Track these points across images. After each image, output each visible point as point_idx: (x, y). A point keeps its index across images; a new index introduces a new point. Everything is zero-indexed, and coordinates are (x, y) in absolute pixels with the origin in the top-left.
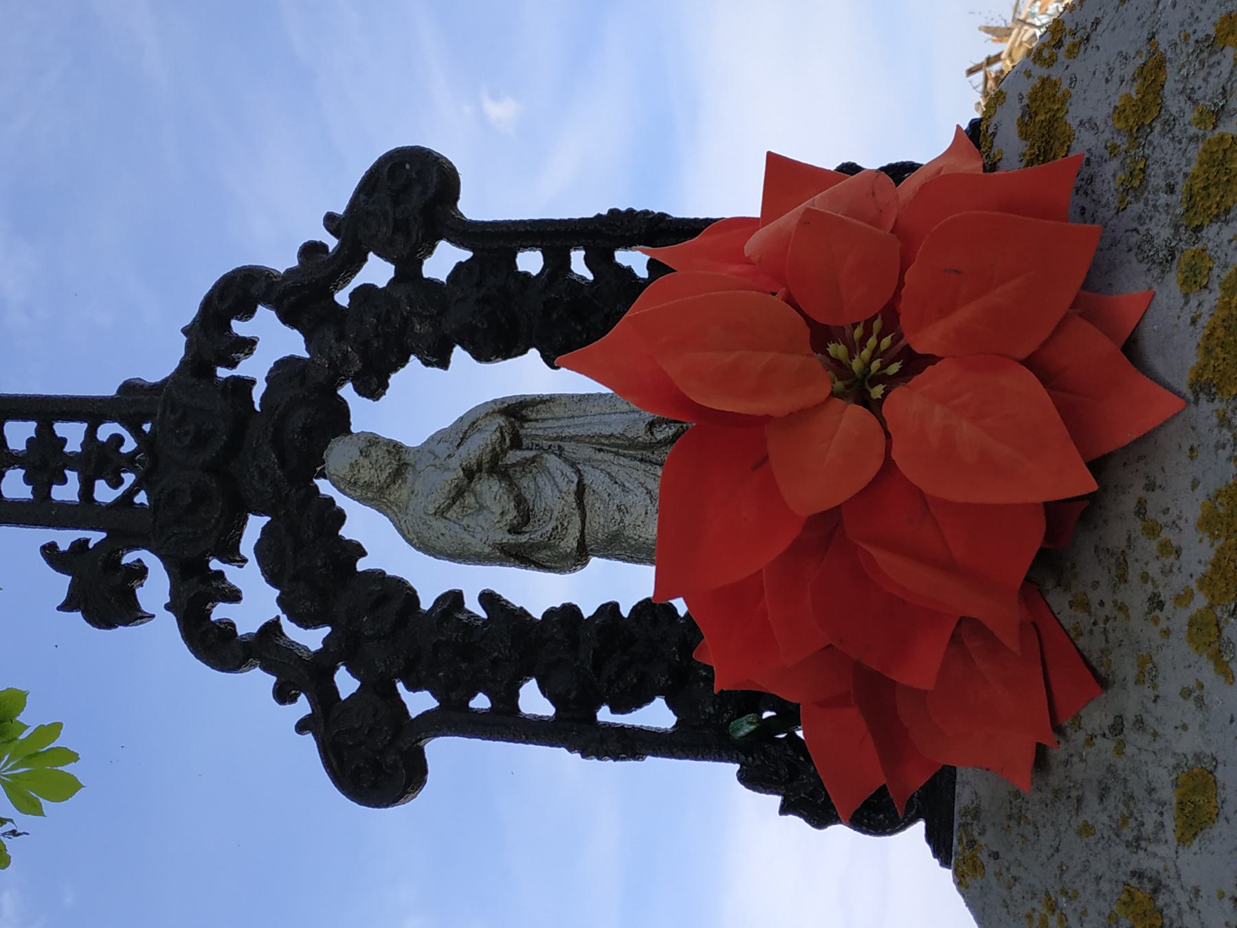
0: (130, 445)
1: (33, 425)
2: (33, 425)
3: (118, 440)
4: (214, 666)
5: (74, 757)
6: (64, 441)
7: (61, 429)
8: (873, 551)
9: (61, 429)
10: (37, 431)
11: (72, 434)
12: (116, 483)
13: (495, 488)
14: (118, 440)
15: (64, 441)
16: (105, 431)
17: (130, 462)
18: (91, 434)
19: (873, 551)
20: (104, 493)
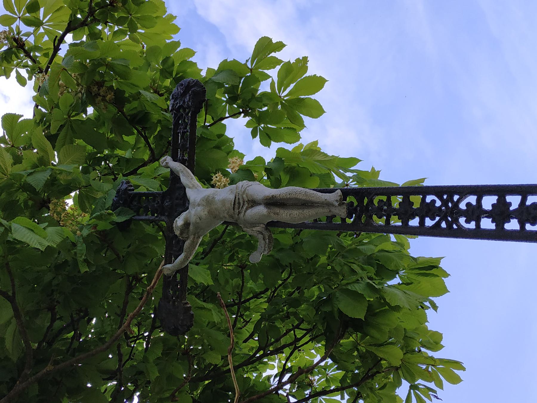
0: (438, 203)
1: (496, 197)
2: (496, 197)
3: (434, 201)
4: (21, 85)
5: (464, 369)
6: (510, 204)
7: (509, 199)
8: (334, 175)
9: (509, 199)
10: (497, 200)
11: (514, 201)
12: (433, 219)
13: (140, 357)
14: (434, 201)
15: (510, 204)
16: (429, 198)
17: (462, 213)
18: (424, 199)
19: (334, 175)
20: (429, 223)
